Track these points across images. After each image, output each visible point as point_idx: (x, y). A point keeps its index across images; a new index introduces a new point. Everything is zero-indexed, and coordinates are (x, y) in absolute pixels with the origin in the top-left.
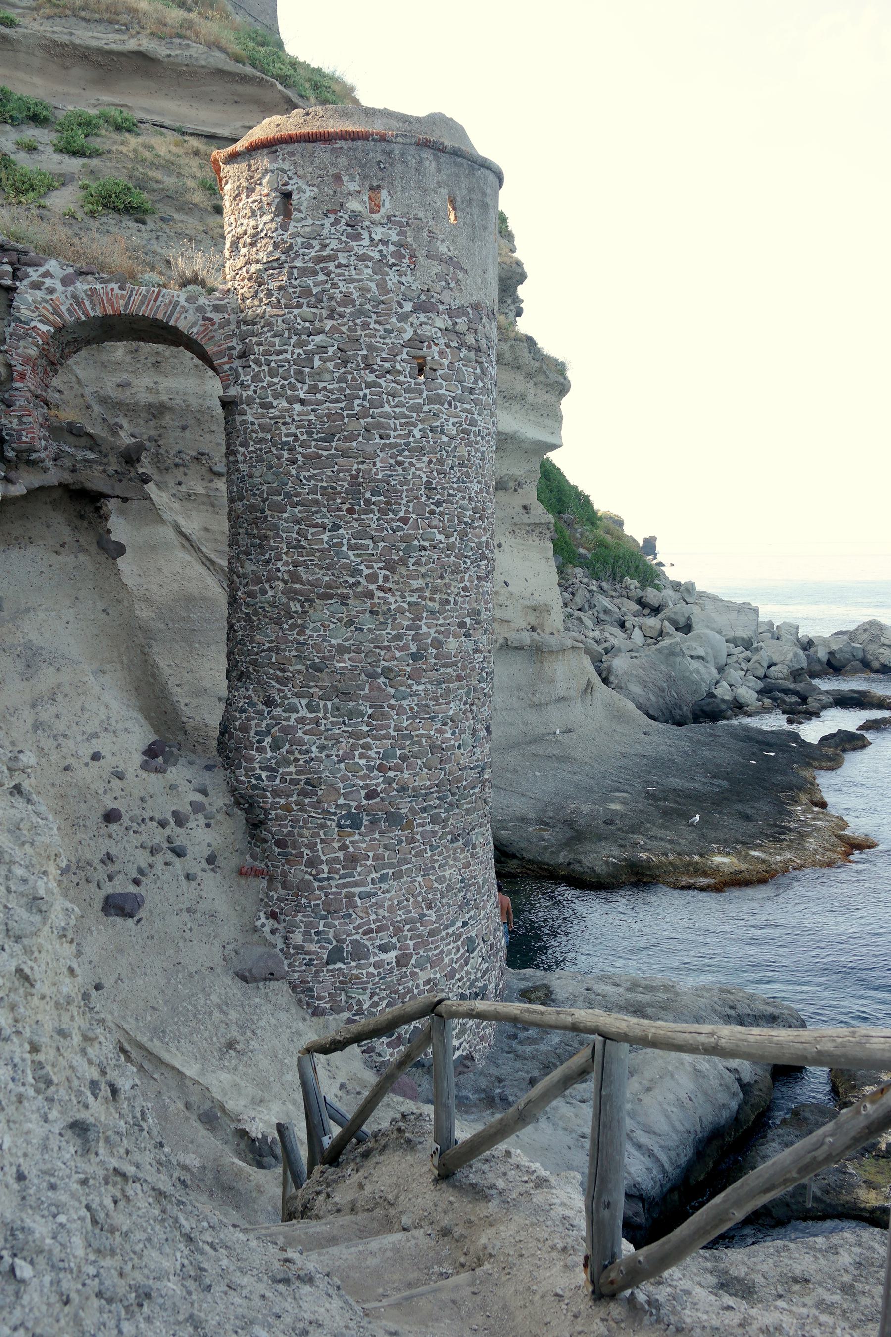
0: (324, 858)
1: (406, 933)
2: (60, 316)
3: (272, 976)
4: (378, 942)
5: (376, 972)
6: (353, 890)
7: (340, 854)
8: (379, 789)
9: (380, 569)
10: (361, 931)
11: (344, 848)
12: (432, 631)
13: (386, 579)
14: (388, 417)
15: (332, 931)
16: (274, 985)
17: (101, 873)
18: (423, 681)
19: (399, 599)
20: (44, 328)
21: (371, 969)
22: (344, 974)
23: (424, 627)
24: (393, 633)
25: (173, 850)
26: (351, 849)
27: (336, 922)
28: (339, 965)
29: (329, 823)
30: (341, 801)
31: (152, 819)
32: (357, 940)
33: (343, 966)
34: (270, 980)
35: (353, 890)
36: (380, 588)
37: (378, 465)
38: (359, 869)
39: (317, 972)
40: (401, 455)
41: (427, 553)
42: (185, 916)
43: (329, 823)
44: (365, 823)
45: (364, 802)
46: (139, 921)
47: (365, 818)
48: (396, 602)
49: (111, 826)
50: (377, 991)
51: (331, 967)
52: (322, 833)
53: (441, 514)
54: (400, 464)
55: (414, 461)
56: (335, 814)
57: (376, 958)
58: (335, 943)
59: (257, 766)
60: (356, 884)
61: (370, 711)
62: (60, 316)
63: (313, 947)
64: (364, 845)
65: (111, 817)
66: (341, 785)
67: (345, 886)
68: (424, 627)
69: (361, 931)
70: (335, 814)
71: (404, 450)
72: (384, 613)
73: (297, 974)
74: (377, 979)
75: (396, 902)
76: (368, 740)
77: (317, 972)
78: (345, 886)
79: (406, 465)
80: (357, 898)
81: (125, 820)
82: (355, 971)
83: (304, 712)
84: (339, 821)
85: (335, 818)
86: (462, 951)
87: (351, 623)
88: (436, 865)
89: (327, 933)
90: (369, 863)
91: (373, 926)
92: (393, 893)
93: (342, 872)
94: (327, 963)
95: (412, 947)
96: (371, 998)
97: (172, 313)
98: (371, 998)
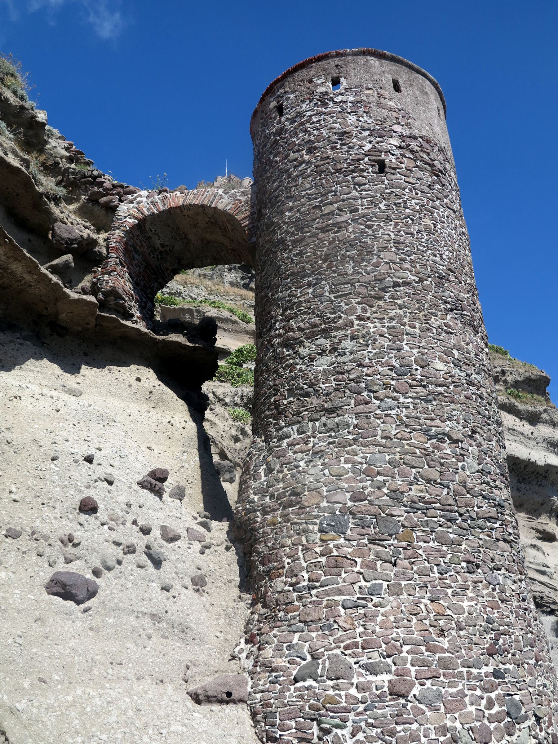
0: (305, 565)
1: (404, 654)
2: (143, 214)
3: (228, 698)
4: (364, 660)
5: (359, 696)
6: (336, 598)
7: (323, 559)
8: (366, 492)
9: (358, 303)
10: (342, 645)
11: (326, 553)
12: (415, 351)
13: (364, 310)
14: (355, 199)
15: (307, 644)
16: (229, 709)
17: (56, 552)
18: (410, 394)
19: (377, 324)
20: (131, 221)
21: (353, 691)
22: (316, 695)
23: (406, 348)
24: (374, 351)
25: (149, 556)
26: (335, 553)
27: (314, 635)
28: (310, 682)
29: (311, 527)
30: (324, 504)
31: (135, 522)
32: (336, 656)
33: (314, 684)
34: (227, 703)
35: (336, 598)
36: (359, 318)
37: (351, 230)
38: (343, 575)
39: (282, 691)
40: (369, 220)
41: (402, 288)
42: (147, 621)
43: (311, 527)
44: (351, 525)
45: (350, 504)
46: (85, 611)
47: (351, 520)
48: (375, 327)
49: (82, 514)
50: (363, 724)
51: (299, 685)
52: (304, 539)
53: (411, 261)
54: (369, 227)
55: (382, 224)
56: (317, 517)
57: (362, 679)
58: (309, 658)
59: (251, 492)
60: (340, 592)
61: (356, 422)
62: (143, 214)
63: (281, 662)
64: (350, 550)
65: (88, 507)
66: (325, 489)
67: (327, 593)
68: (406, 348)
69: (342, 645)
70: (317, 517)
71: (371, 218)
72: (364, 337)
73: (258, 696)
74: (361, 707)
75: (392, 618)
76: (354, 447)
77: (282, 691)
78: (327, 593)
79: (375, 227)
80: (340, 607)
81: (102, 515)
82: (331, 692)
83: (295, 436)
84: (321, 524)
85: (318, 521)
86: (496, 709)
87: (334, 349)
88: (449, 591)
89: (302, 647)
90: (356, 570)
91: (359, 640)
92: (388, 608)
93: (323, 578)
94: (296, 681)
95: (413, 674)
96: (353, 735)
97: (214, 200)
98: (353, 735)
